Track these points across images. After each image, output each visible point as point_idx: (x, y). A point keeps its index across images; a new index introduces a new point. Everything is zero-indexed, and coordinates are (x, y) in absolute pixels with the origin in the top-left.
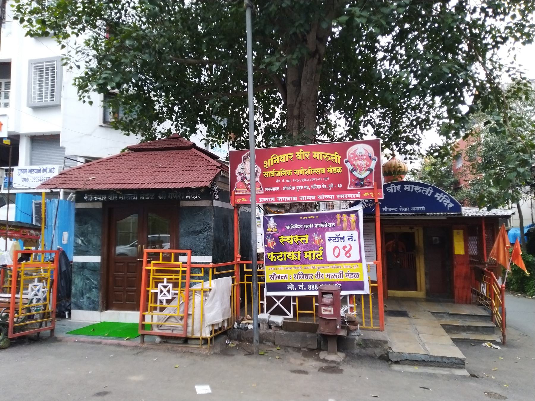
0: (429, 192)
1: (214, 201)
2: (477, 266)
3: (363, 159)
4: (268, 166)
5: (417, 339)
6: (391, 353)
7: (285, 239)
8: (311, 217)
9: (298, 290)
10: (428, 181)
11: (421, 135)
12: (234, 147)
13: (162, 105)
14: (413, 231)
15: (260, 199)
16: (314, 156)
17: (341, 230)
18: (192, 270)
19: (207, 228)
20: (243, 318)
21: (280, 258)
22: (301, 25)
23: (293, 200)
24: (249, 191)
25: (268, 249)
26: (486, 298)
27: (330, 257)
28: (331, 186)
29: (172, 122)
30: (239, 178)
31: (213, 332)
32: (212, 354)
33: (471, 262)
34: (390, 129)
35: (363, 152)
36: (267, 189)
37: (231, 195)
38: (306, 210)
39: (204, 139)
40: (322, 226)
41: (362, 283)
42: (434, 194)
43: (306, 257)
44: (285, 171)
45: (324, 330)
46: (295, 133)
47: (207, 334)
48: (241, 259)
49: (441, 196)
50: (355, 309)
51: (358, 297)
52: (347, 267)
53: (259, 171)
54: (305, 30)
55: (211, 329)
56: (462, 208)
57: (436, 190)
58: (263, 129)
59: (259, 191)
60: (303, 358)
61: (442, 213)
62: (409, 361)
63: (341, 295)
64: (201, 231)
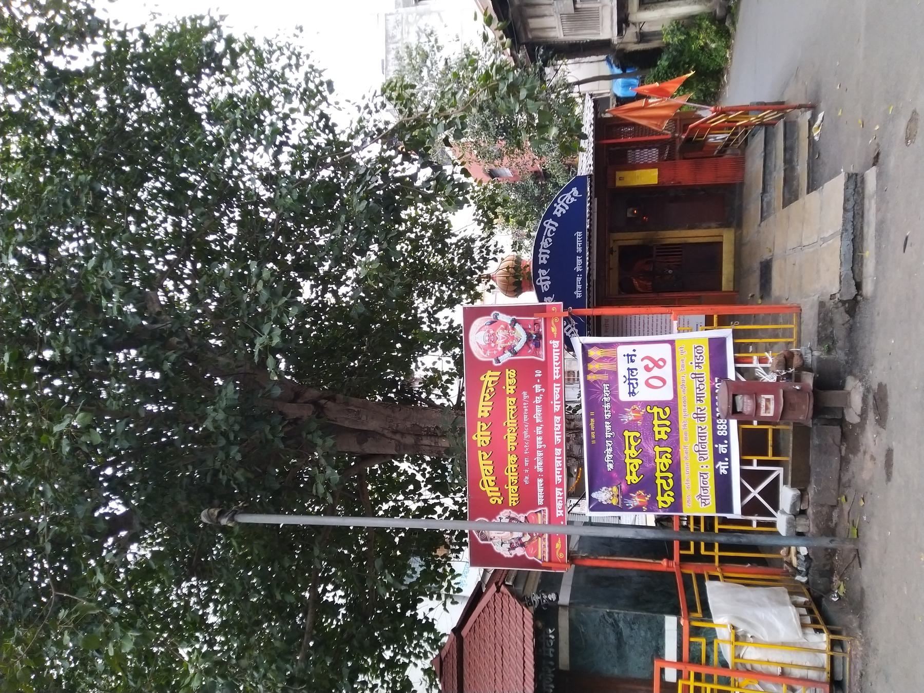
0: (551, 225)
1: (560, 602)
2: (678, 148)
3: (494, 334)
4: (499, 497)
5: (811, 250)
6: (841, 296)
7: (631, 472)
8: (592, 424)
9: (728, 455)
10: (533, 226)
11: (458, 238)
12: (461, 550)
13: (379, 682)
14: (616, 249)
15: (558, 515)
16: (486, 415)
17: (615, 373)
18: (695, 659)
19: (610, 620)
20: (786, 562)
21: (668, 485)
22: (273, 428)
23: (562, 455)
24: (541, 535)
25: (651, 506)
26: (735, 134)
27: (666, 394)
28: (538, 388)
29: (411, 665)
30: (519, 551)
31: (818, 626)
32: (863, 632)
33: (671, 157)
34: (444, 282)
35: (482, 333)
36: (540, 501)
37: (550, 568)
38: (577, 429)
39: (444, 604)
40: (607, 406)
41: (711, 340)
42: (555, 218)
43: (665, 437)
44: (509, 467)
45: (804, 413)
46: (444, 443)
47: (822, 640)
48: (670, 558)
49: (558, 207)
50: (761, 355)
51: (737, 348)
52: (683, 366)
53: (507, 514)
54: (280, 424)
55: (810, 631)
56: (579, 174)
57: (550, 215)
58: (434, 496)
59: (544, 516)
60: (860, 455)
61: (588, 205)
62: (856, 265)
63: (737, 378)
64: (617, 634)
